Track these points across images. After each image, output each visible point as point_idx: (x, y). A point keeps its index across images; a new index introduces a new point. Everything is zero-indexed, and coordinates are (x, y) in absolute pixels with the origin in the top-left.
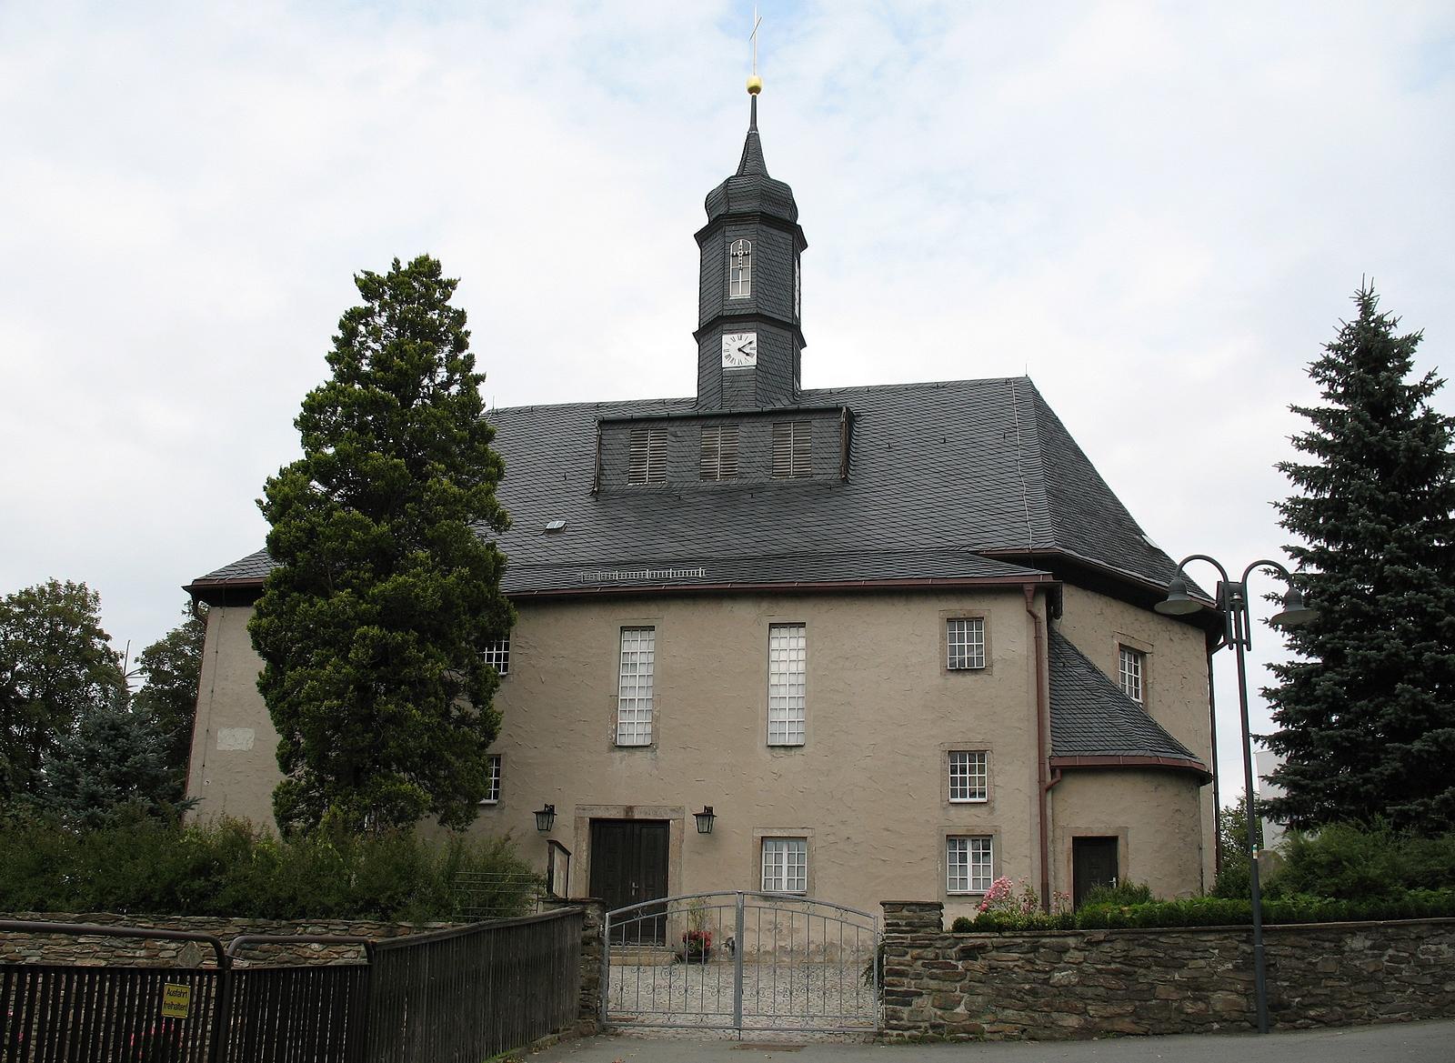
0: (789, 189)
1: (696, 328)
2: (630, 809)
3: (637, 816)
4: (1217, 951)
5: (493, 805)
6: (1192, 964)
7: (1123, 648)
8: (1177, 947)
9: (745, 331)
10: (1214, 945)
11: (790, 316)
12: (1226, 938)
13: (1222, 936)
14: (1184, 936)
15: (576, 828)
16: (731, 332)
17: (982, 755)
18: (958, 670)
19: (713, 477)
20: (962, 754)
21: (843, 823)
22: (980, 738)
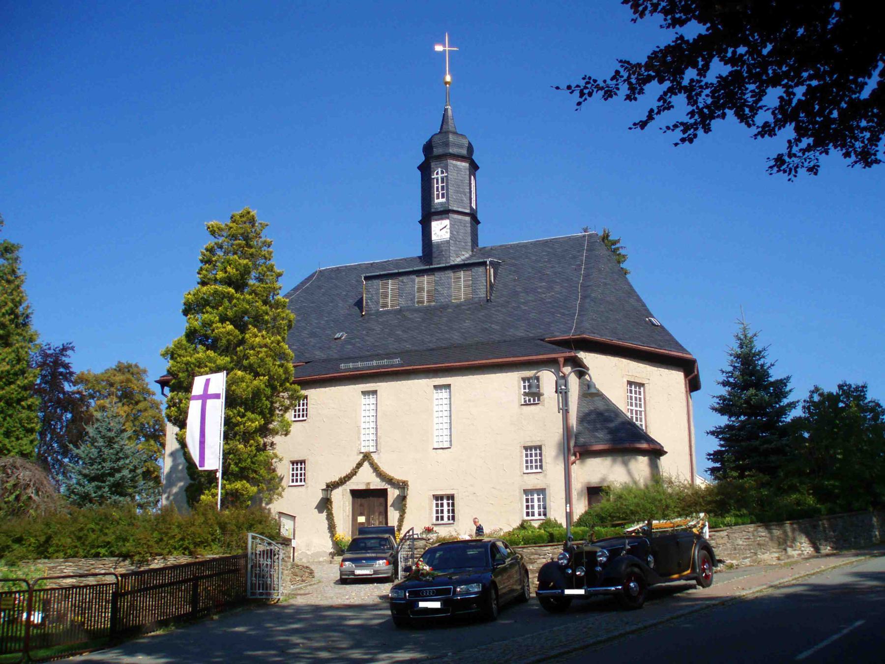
0: (424, 145)
1: (420, 218)
2: (368, 484)
3: (372, 488)
4: (550, 555)
5: (303, 485)
6: (539, 561)
7: (630, 383)
8: (532, 554)
9: (442, 219)
10: (549, 552)
11: (469, 208)
12: (556, 548)
13: (554, 547)
14: (535, 548)
15: (343, 495)
16: (436, 220)
17: (540, 448)
18: (527, 405)
19: (423, 302)
20: (531, 448)
21: (472, 486)
22: (539, 439)
